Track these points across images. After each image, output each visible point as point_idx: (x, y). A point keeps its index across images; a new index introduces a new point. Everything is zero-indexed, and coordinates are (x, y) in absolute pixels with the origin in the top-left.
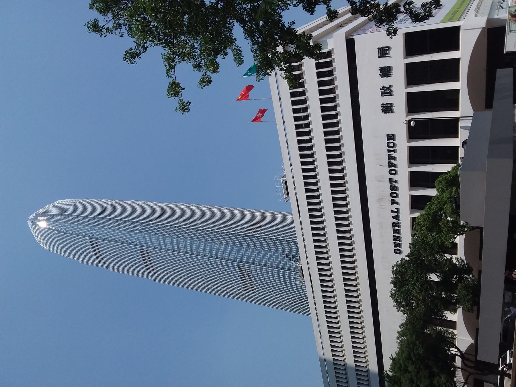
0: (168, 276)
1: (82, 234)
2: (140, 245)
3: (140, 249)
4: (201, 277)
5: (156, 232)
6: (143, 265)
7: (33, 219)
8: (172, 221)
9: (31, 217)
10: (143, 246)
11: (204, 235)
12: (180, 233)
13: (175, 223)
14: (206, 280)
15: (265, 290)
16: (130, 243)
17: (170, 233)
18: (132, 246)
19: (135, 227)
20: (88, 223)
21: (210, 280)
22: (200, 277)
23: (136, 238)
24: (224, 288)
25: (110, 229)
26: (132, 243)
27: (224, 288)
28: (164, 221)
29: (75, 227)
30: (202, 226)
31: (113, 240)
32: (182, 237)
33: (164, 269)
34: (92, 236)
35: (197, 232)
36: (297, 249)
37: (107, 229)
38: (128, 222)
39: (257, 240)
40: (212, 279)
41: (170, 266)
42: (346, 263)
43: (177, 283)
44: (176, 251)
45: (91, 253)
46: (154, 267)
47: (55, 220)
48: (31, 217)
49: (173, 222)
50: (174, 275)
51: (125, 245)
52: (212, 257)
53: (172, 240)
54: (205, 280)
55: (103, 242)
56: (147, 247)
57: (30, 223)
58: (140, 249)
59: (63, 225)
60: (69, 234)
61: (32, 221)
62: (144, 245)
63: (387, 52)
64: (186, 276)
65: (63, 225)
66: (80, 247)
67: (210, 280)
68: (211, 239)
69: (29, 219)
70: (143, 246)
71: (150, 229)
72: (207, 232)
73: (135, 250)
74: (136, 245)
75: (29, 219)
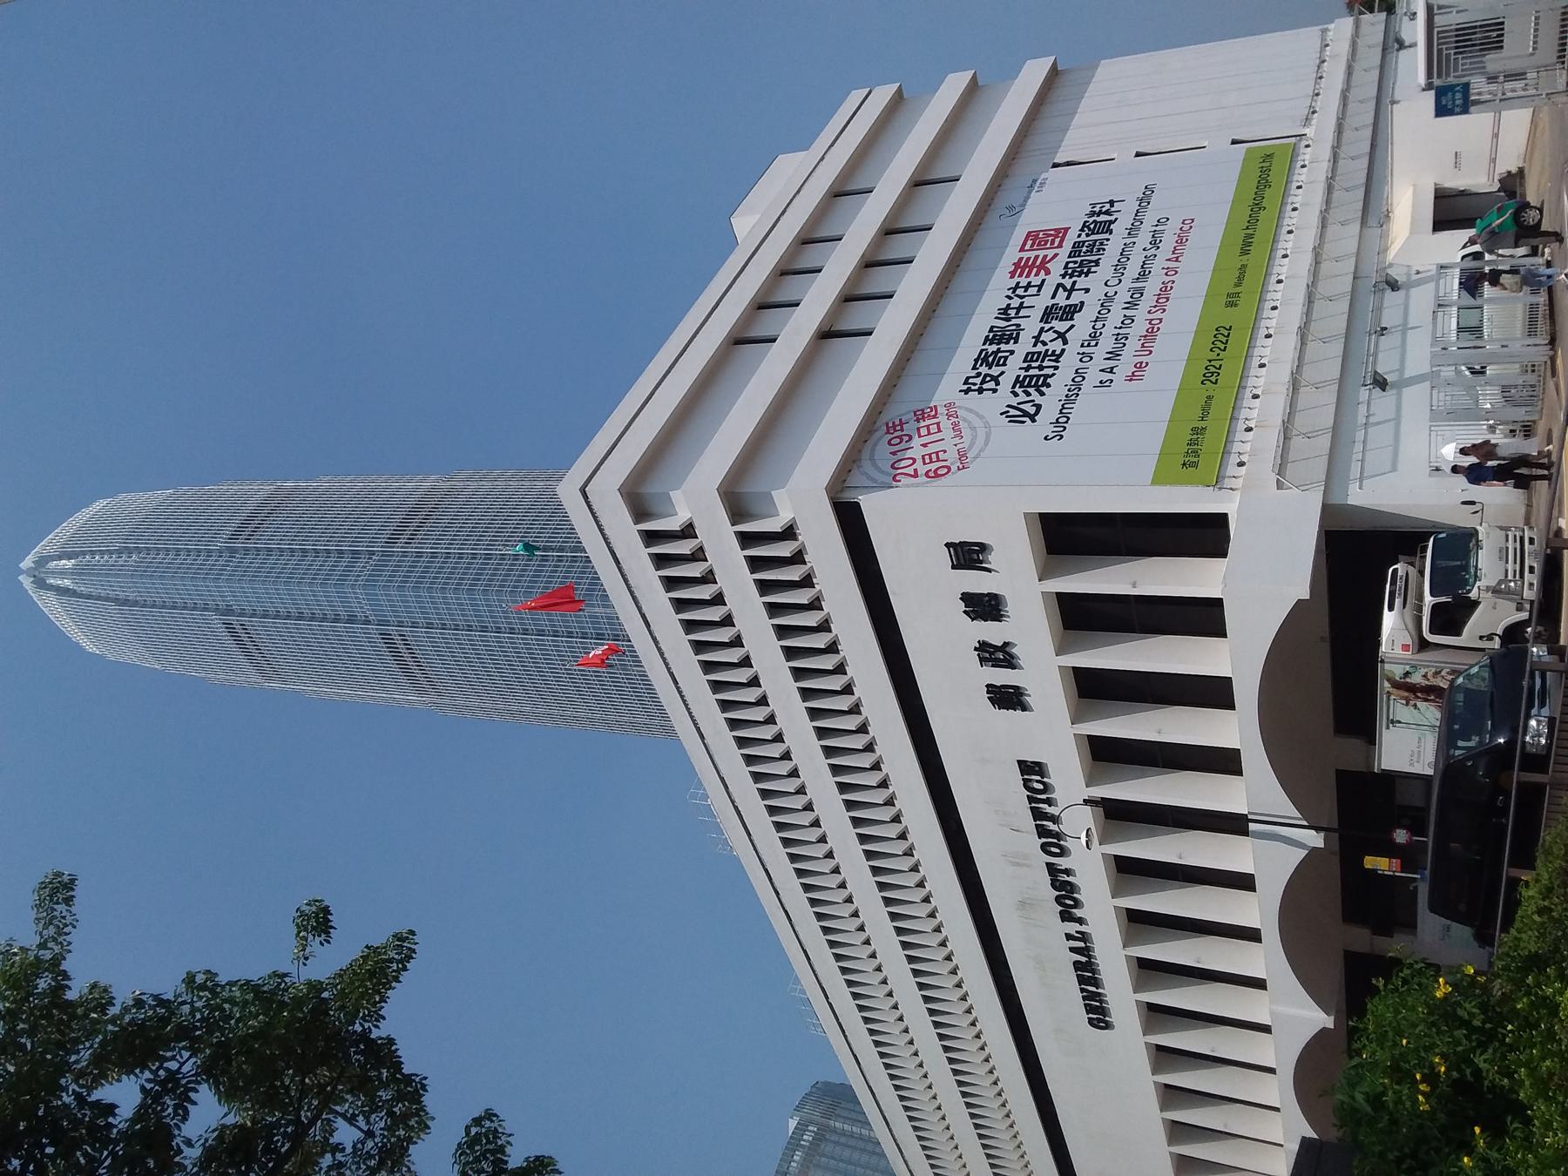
0: (463, 673)
1: (195, 604)
2: (379, 620)
3: (381, 634)
4: (543, 680)
5: (330, 570)
6: (388, 657)
7: (35, 569)
8: (501, 520)
9: (27, 563)
10: (387, 623)
11: (425, 567)
12: (466, 568)
13: (463, 536)
14: (572, 682)
15: (622, 687)
16: (363, 618)
17: (393, 571)
18: (353, 628)
19: (350, 566)
20: (143, 567)
21: (644, 693)
22: (599, 689)
23: (359, 601)
24: (596, 692)
25: (311, 585)
26: (352, 619)
27: (596, 692)
28: (502, 524)
29: (166, 584)
30: (489, 536)
31: (258, 612)
32: (325, 579)
33: (509, 673)
34: (225, 607)
35: (488, 564)
36: (593, 578)
37: (267, 583)
38: (291, 552)
39: (482, 564)
40: (531, 675)
41: (490, 664)
42: (689, 604)
43: (343, 664)
44: (503, 630)
45: (220, 632)
46: (424, 662)
47: (101, 570)
48: (27, 563)
49: (476, 523)
50: (486, 679)
51: (331, 626)
52: (484, 629)
53: (470, 599)
54: (644, 693)
55: (300, 625)
56: (400, 624)
57: (26, 582)
58: (381, 634)
59: (130, 582)
60: (163, 607)
61: (35, 576)
62: (388, 621)
63: (810, 1131)
64: (523, 674)
65: (130, 582)
66: (185, 626)
67: (552, 681)
68: (530, 581)
69: (21, 572)
70: (387, 623)
71: (400, 566)
72: (501, 559)
73: (484, 646)
74: (367, 622)
75: (21, 572)
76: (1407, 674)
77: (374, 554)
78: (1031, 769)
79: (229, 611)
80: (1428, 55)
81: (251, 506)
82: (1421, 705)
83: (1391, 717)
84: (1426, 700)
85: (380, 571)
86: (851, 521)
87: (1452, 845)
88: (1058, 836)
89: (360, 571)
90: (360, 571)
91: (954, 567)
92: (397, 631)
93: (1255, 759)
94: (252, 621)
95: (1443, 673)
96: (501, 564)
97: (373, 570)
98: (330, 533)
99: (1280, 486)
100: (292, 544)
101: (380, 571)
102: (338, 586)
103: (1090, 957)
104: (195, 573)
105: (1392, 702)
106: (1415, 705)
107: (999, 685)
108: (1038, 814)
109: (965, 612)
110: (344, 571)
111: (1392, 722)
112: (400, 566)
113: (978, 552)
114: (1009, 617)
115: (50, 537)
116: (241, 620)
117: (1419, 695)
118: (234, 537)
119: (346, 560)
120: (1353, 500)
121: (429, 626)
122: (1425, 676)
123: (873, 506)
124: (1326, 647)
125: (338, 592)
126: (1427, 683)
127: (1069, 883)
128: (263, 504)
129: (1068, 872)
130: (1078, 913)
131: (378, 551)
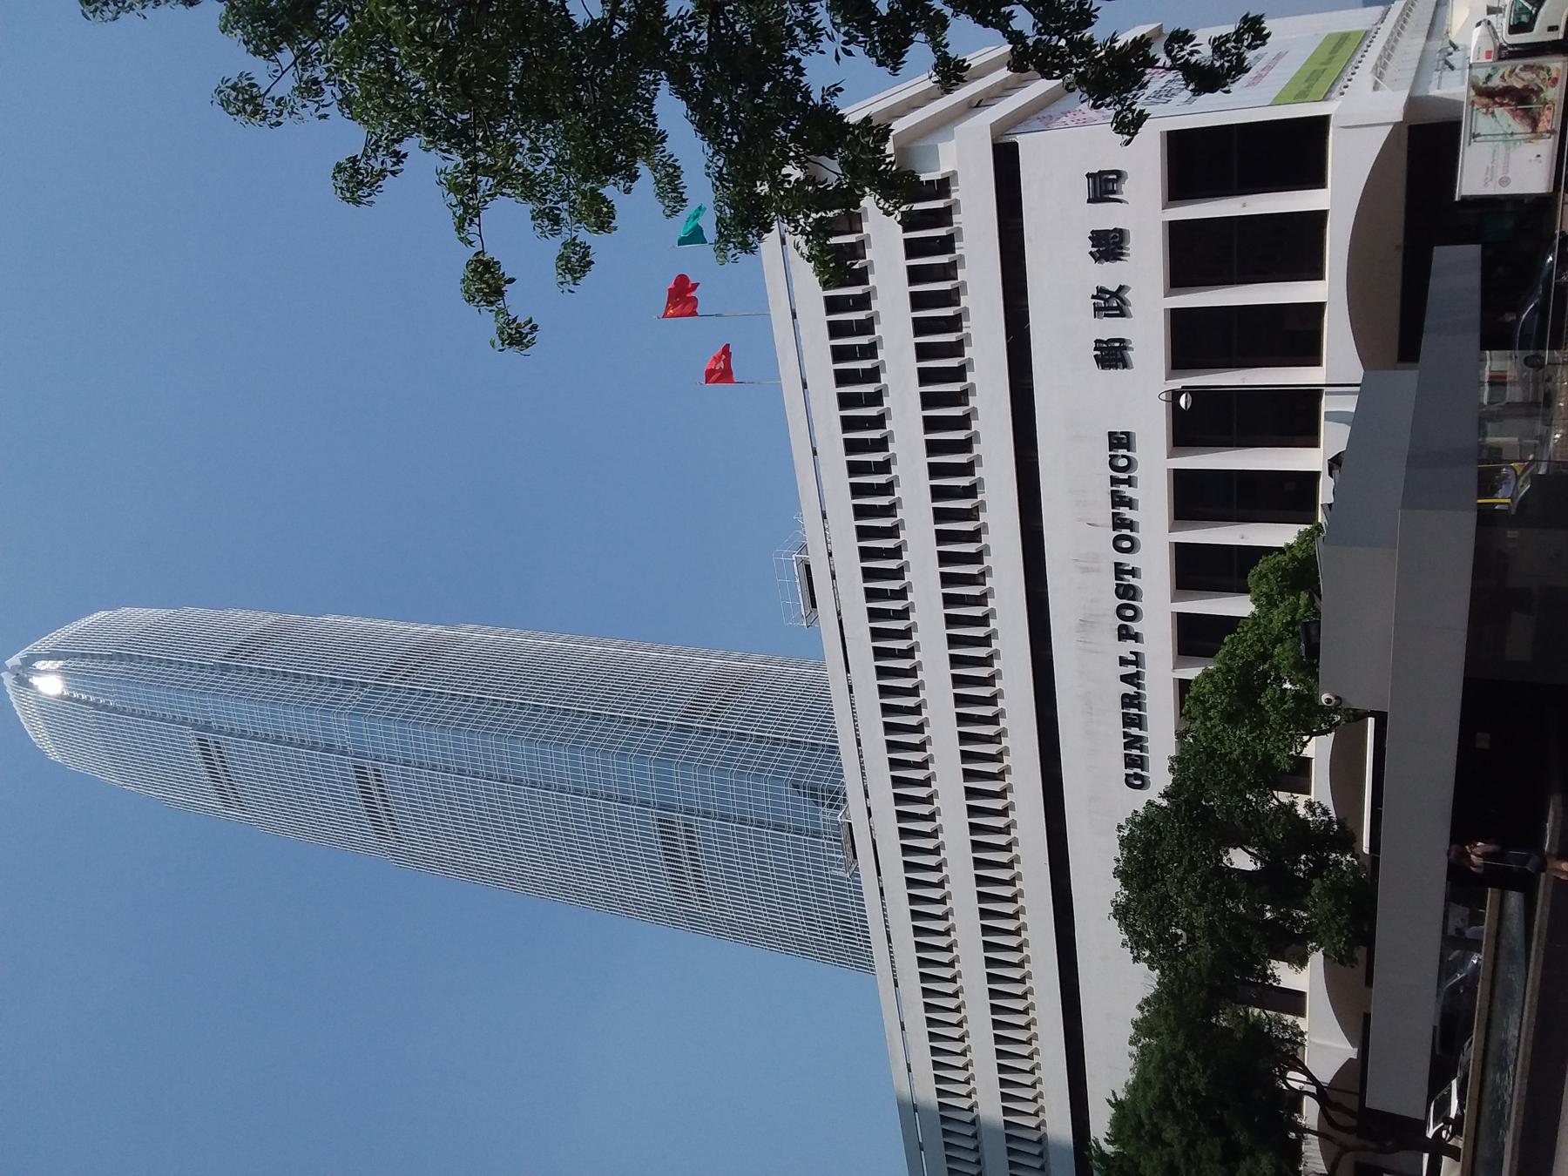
7: (20, 668)
9: (14, 661)
23: (342, 733)
24: (555, 874)
26: (329, 748)
48: (14, 661)
57: (8, 680)
69: (5, 669)
75: (5, 669)
76: (1489, 77)
77: (365, 687)
78: (1120, 441)
79: (207, 727)
80: (1363, 1051)
81: (253, 629)
82: (1498, 111)
83: (1473, 131)
84: (1502, 105)
85: (369, 702)
86: (1006, 161)
87: (1426, 1156)
88: (1131, 525)
89: (346, 705)
90: (346, 705)
91: (1089, 201)
92: (372, 765)
93: (1337, 333)
94: (228, 740)
95: (1517, 70)
96: (492, 709)
97: (358, 705)
98: (323, 665)
99: (1376, 87)
100: (287, 668)
101: (369, 702)
102: (324, 713)
103: (1138, 686)
104: (182, 686)
105: (1474, 113)
106: (1493, 113)
107: (1106, 340)
108: (1118, 500)
109: (1091, 253)
110: (332, 699)
111: (1474, 136)
112: (383, 709)
113: (1113, 181)
114: (1129, 255)
115: (36, 643)
116: (217, 738)
117: (1496, 99)
118: (230, 655)
119: (338, 688)
120: (1434, 92)
121: (407, 763)
122: (1502, 77)
123: (1029, 146)
124: (1400, 255)
125: (321, 719)
126: (1505, 85)
127: (1132, 587)
128: (263, 631)
129: (1133, 572)
130: (1135, 627)
131: (371, 684)
